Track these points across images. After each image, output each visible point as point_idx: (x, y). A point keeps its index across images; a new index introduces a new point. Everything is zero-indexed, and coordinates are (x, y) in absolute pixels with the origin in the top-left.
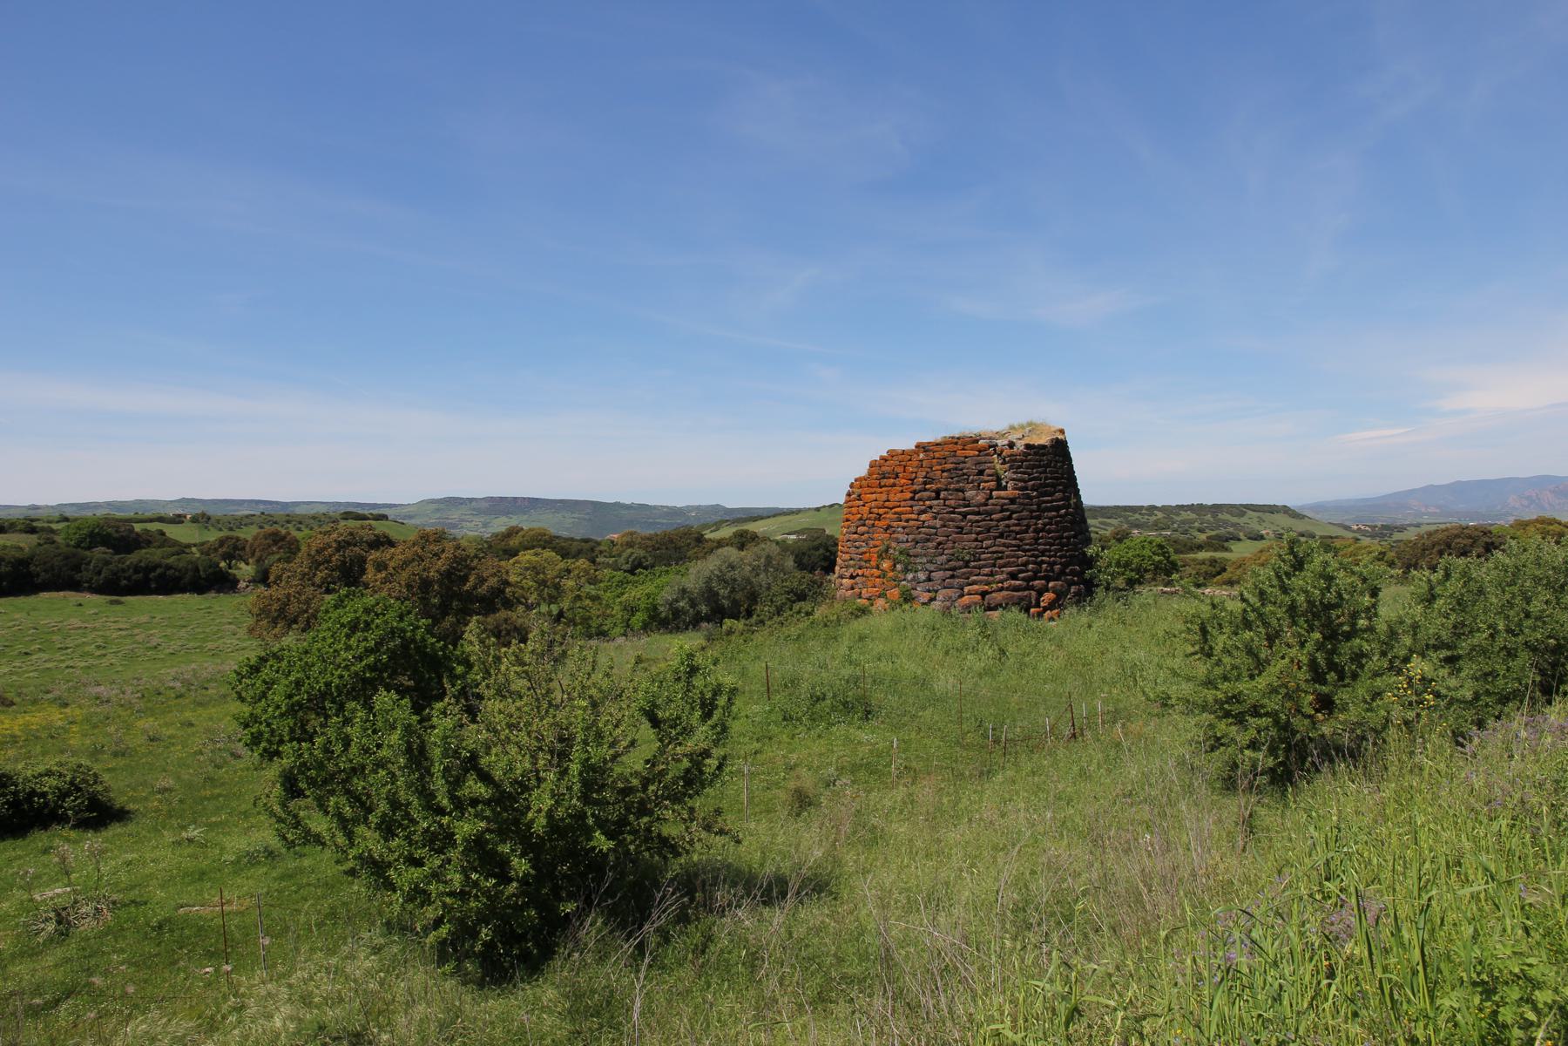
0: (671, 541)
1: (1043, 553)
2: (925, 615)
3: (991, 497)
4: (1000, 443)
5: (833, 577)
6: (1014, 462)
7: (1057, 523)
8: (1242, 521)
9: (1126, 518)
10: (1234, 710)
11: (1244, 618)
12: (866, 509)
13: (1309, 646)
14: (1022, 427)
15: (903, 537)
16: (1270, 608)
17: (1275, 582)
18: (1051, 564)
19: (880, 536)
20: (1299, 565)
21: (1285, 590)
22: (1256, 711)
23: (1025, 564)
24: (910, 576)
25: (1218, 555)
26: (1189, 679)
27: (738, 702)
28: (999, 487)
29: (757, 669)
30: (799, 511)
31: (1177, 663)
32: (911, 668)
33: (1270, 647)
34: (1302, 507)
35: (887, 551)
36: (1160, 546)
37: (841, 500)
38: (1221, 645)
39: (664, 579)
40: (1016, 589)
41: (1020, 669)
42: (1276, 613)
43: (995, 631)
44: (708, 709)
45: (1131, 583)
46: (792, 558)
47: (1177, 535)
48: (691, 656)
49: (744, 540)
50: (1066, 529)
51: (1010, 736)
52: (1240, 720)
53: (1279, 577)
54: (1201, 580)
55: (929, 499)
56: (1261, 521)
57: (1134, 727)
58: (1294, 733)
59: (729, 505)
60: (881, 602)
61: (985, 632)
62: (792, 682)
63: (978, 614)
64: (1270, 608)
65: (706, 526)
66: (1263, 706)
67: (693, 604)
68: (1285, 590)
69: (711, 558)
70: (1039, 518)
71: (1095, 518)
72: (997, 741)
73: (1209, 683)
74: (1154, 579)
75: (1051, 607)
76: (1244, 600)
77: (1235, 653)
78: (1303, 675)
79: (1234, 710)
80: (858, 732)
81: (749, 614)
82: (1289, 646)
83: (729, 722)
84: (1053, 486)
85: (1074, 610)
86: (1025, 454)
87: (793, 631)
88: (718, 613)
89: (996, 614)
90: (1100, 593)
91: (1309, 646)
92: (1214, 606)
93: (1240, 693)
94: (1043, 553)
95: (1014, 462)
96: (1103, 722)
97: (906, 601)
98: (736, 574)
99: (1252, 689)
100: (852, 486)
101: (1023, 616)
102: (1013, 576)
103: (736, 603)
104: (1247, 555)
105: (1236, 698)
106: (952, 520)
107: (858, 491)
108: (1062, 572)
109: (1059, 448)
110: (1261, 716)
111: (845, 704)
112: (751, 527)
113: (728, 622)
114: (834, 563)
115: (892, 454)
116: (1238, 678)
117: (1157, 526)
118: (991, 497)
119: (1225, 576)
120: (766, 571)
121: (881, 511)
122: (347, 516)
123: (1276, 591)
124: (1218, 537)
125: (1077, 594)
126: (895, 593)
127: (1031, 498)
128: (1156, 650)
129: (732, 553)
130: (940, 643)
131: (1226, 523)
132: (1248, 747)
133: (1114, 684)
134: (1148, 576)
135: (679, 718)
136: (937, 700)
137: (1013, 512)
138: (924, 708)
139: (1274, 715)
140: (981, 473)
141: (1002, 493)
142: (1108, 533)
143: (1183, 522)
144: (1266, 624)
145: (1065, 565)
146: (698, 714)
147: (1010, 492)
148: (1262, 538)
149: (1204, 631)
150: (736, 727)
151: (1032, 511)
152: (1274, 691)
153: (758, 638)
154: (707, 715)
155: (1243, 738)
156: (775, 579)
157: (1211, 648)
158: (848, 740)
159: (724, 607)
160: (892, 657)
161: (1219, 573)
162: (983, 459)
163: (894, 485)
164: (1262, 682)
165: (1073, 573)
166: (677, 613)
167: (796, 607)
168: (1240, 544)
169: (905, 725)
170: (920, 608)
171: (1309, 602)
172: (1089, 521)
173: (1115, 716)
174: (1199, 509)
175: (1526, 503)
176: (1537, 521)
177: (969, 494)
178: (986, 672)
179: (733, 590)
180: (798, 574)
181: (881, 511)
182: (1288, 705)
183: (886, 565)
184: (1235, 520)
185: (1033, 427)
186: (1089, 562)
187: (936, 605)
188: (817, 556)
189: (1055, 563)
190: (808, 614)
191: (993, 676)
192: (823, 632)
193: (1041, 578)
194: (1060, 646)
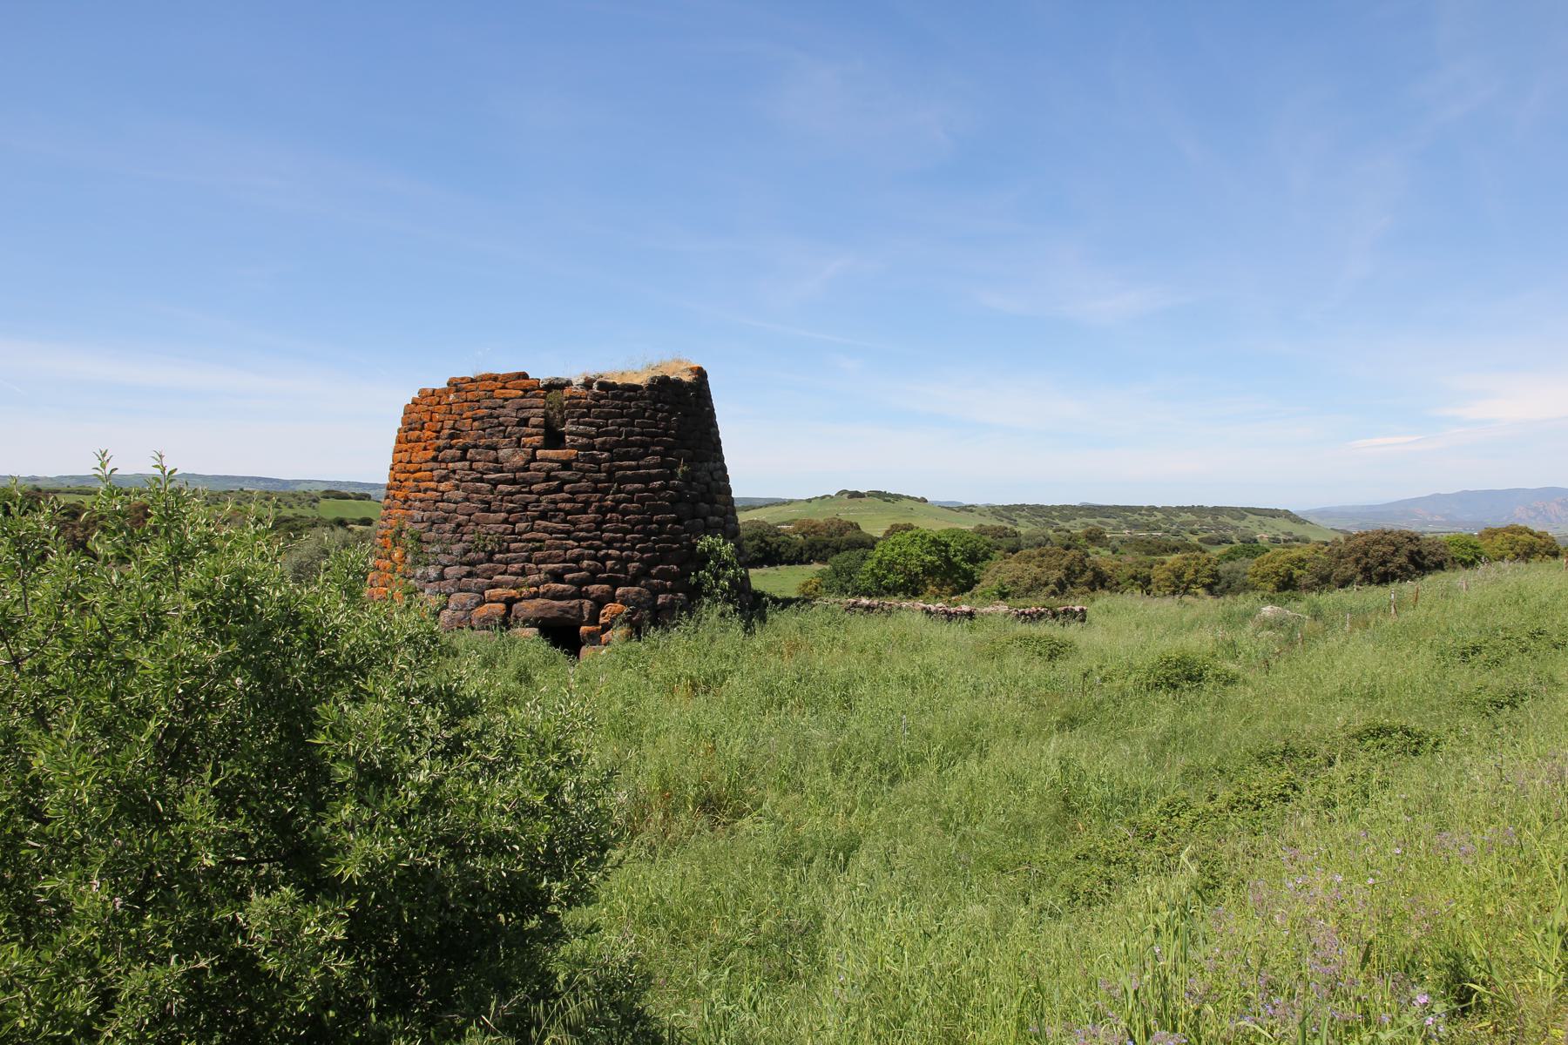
1: (609, 544)
3: (534, 459)
7: (641, 501)
9: (1125, 518)
23: (577, 560)
30: (791, 502)
34: (1307, 512)
55: (454, 460)
84: (642, 445)
102: (557, 577)
106: (478, 491)
108: (644, 573)
117: (1148, 527)
118: (534, 459)
122: (329, 494)
127: (598, 462)
131: (1226, 526)
137: (564, 482)
143: (1182, 524)
162: (527, 402)
163: (418, 440)
165: (663, 575)
174: (1199, 511)
175: (1532, 514)
176: (1507, 530)
184: (1236, 523)
193: (603, 581)
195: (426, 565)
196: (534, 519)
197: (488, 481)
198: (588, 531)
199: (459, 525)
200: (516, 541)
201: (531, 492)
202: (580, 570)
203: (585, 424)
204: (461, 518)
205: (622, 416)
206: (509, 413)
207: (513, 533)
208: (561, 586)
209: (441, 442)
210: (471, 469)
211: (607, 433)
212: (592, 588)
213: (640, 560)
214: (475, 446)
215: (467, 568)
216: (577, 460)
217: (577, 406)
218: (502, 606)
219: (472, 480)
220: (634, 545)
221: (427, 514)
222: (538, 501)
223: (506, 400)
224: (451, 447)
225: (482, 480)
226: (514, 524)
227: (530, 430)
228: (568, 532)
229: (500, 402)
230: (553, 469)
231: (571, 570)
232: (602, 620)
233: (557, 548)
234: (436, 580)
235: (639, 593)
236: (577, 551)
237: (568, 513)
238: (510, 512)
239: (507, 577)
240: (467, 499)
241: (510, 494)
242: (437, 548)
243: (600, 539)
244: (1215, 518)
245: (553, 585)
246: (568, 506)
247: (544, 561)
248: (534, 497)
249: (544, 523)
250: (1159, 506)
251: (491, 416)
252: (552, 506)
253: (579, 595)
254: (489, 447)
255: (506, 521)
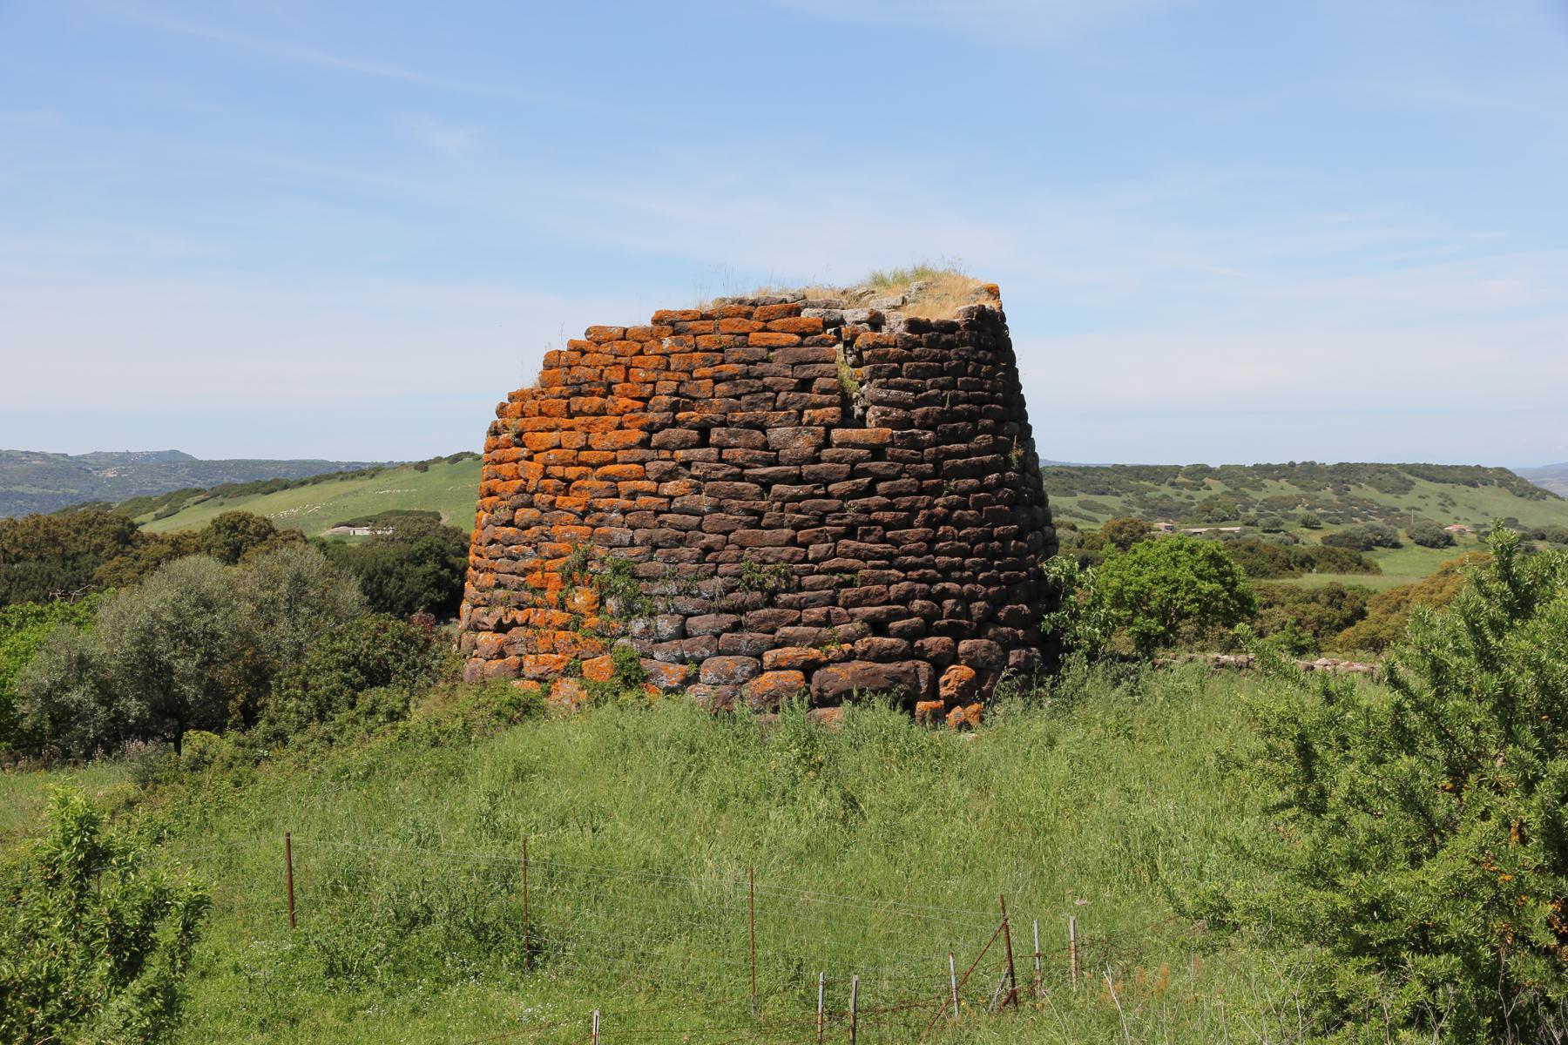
0: (54, 541)
1: (946, 572)
2: (672, 717)
3: (827, 443)
4: (850, 315)
5: (456, 628)
6: (882, 362)
7: (978, 505)
8: (1403, 502)
9: (1140, 494)
10: (1374, 936)
11: (1398, 725)
12: (535, 468)
13: (1545, 791)
14: (902, 280)
15: (624, 535)
16: (1455, 702)
17: (1467, 643)
18: (966, 600)
19: (568, 531)
20: (1522, 604)
21: (1489, 661)
22: (1423, 940)
23: (905, 599)
24: (637, 626)
25: (1348, 580)
26: (1271, 864)
27: (212, 940)
28: (848, 419)
29: (264, 852)
30: (376, 470)
31: (1247, 828)
32: (637, 841)
33: (1457, 791)
34: (1543, 471)
35: (584, 566)
36: (1215, 560)
37: (477, 443)
38: (1344, 785)
39: (32, 634)
40: (884, 657)
41: (889, 843)
42: (1470, 714)
43: (834, 756)
44: (130, 953)
45: (1147, 643)
46: (355, 583)
47: (1254, 534)
48: (88, 823)
49: (238, 540)
50: (998, 519)
51: (866, 1000)
52: (1388, 960)
53: (1475, 631)
54: (1307, 637)
55: (685, 445)
56: (1447, 503)
57: (1153, 975)
58: (1510, 990)
59: (202, 455)
60: (569, 686)
61: (813, 758)
62: (352, 881)
63: (796, 714)
64: (1455, 702)
65: (143, 504)
66: (1440, 928)
67: (106, 694)
68: (1489, 661)
69: (154, 581)
70: (936, 491)
71: (1069, 492)
72: (835, 1013)
73: (1319, 875)
74: (1200, 635)
75: (964, 696)
76: (1396, 683)
77: (1375, 803)
78: (1532, 856)
79: (1374, 936)
80: (509, 1000)
81: (249, 717)
82: (1497, 788)
83: (189, 984)
84: (972, 417)
85: (1017, 704)
86: (910, 345)
87: (356, 757)
88: (170, 718)
89: (836, 715)
90: (1075, 665)
91: (1545, 791)
92: (1329, 697)
93: (1389, 895)
94: (946, 572)
95: (882, 362)
96: (1081, 968)
97: (628, 682)
98: (218, 621)
99: (1416, 887)
100: (501, 411)
101: (898, 719)
102: (878, 627)
103: (214, 691)
104: (1415, 581)
105: (1378, 909)
106: (738, 495)
107: (515, 424)
108: (990, 619)
109: (988, 330)
110: (1436, 951)
111: (479, 931)
112: (258, 507)
113: (195, 739)
114: (457, 595)
115: (598, 337)
116: (1384, 863)
117: (1210, 513)
118: (827, 443)
119: (1363, 628)
120: (292, 612)
121: (571, 472)
123: (1469, 663)
124: (1350, 540)
125: (1025, 668)
126: (601, 666)
128: (1200, 798)
129: (207, 570)
130: (707, 779)
131: (1367, 508)
132: (1408, 1023)
133: (1105, 878)
134: (1186, 627)
135: (54, 978)
136: (694, 920)
138: (667, 938)
139: (1463, 948)
140: (805, 385)
141: (854, 434)
142: (1098, 529)
143: (1270, 504)
144: (1447, 739)
145: (996, 602)
146: (104, 966)
147: (872, 432)
148: (1448, 541)
149: (1306, 754)
150: (203, 996)
151: (921, 477)
152: (1466, 892)
153: (268, 775)
154: (128, 969)
155: (1397, 1002)
156: (315, 631)
157: (1323, 794)
158: (485, 1018)
159: (185, 702)
160: (593, 818)
161: (1349, 622)
162: (808, 353)
163: (602, 411)
164: (1437, 872)
165: (1014, 620)
166: (63, 718)
167: (365, 699)
168: (1398, 556)
169: (621, 979)
170: (660, 701)
171: (1544, 689)
172: (1053, 500)
173: (1107, 949)
174: (1305, 474)
177: (776, 435)
178: (814, 850)
179: (209, 660)
180: (371, 621)
181: (571, 472)
182: (1498, 924)
183: (581, 599)
184: (1387, 500)
185: (927, 281)
186: (1051, 595)
187: (695, 693)
188: (419, 580)
189: (973, 597)
190: (393, 716)
191: (828, 860)
192: (427, 759)
193: (941, 632)
194: (983, 790)
195: (652, 615)
196: (837, 537)
197: (754, 479)
198: (918, 555)
199: (708, 550)
200: (811, 573)
201: (828, 496)
202: (910, 615)
203: (898, 387)
204: (710, 538)
205: (942, 373)
206: (779, 369)
207: (805, 560)
208: (887, 641)
209: (654, 417)
210: (721, 460)
211: (927, 401)
212: (930, 642)
213: (986, 598)
214: (723, 424)
215: (733, 618)
216: (892, 444)
217: (883, 358)
218: (799, 675)
219: (724, 478)
220: (976, 574)
221: (640, 534)
222: (841, 509)
223: (771, 349)
224: (675, 424)
225: (741, 478)
226: (805, 545)
227: (817, 398)
228: (890, 557)
229: (762, 352)
230: (859, 459)
231: (898, 616)
232: (943, 692)
233: (877, 582)
234: (671, 638)
235: (989, 648)
236: (904, 585)
237: (888, 527)
238: (797, 527)
239: (801, 630)
240: (719, 509)
241: (796, 498)
242: (672, 588)
243: (934, 566)
244: (1341, 491)
245: (877, 640)
246: (887, 516)
247: (857, 603)
248: (835, 503)
249: (854, 544)
250: (1215, 463)
251: (747, 375)
252: (863, 517)
253: (912, 654)
254: (750, 425)
255: (792, 541)
